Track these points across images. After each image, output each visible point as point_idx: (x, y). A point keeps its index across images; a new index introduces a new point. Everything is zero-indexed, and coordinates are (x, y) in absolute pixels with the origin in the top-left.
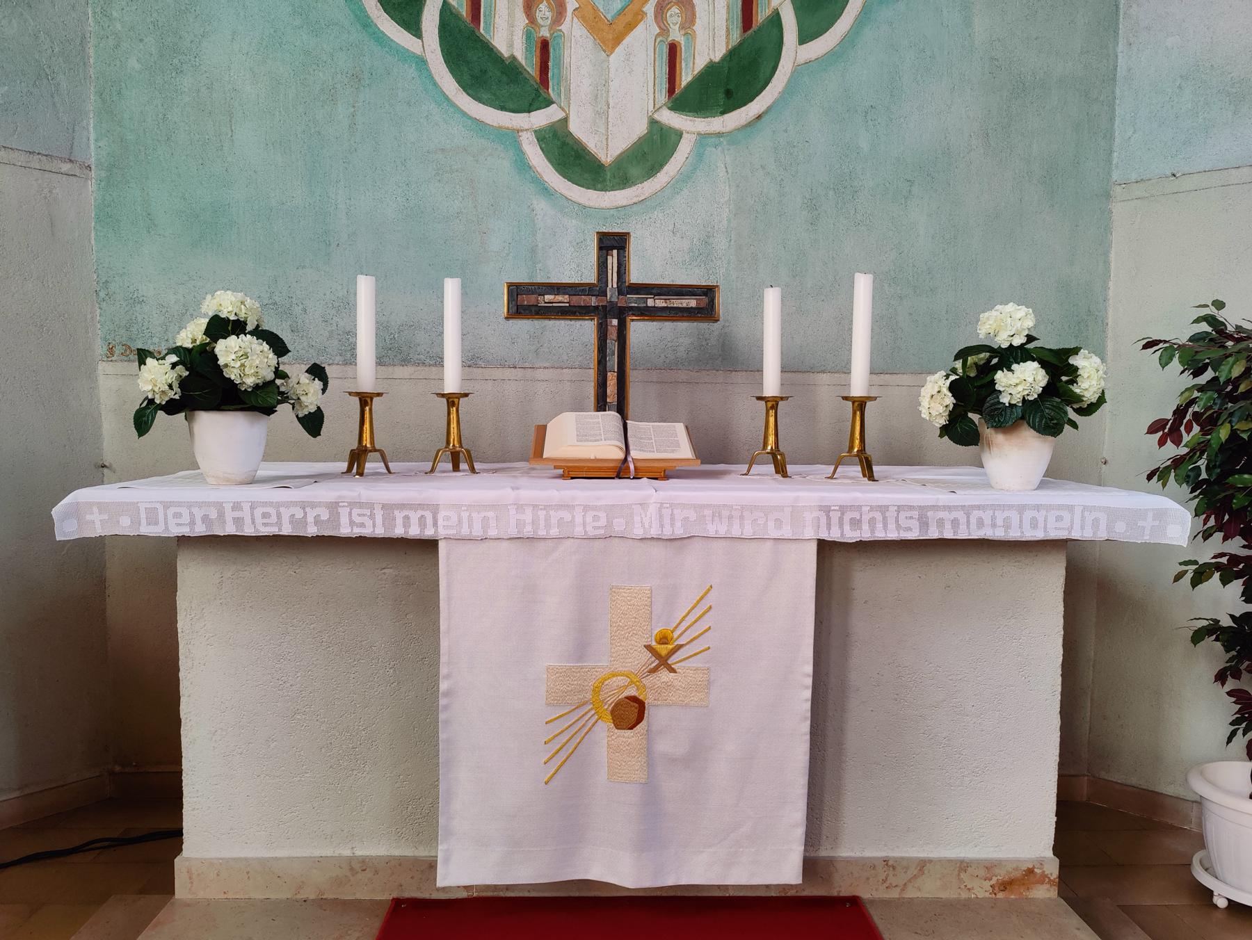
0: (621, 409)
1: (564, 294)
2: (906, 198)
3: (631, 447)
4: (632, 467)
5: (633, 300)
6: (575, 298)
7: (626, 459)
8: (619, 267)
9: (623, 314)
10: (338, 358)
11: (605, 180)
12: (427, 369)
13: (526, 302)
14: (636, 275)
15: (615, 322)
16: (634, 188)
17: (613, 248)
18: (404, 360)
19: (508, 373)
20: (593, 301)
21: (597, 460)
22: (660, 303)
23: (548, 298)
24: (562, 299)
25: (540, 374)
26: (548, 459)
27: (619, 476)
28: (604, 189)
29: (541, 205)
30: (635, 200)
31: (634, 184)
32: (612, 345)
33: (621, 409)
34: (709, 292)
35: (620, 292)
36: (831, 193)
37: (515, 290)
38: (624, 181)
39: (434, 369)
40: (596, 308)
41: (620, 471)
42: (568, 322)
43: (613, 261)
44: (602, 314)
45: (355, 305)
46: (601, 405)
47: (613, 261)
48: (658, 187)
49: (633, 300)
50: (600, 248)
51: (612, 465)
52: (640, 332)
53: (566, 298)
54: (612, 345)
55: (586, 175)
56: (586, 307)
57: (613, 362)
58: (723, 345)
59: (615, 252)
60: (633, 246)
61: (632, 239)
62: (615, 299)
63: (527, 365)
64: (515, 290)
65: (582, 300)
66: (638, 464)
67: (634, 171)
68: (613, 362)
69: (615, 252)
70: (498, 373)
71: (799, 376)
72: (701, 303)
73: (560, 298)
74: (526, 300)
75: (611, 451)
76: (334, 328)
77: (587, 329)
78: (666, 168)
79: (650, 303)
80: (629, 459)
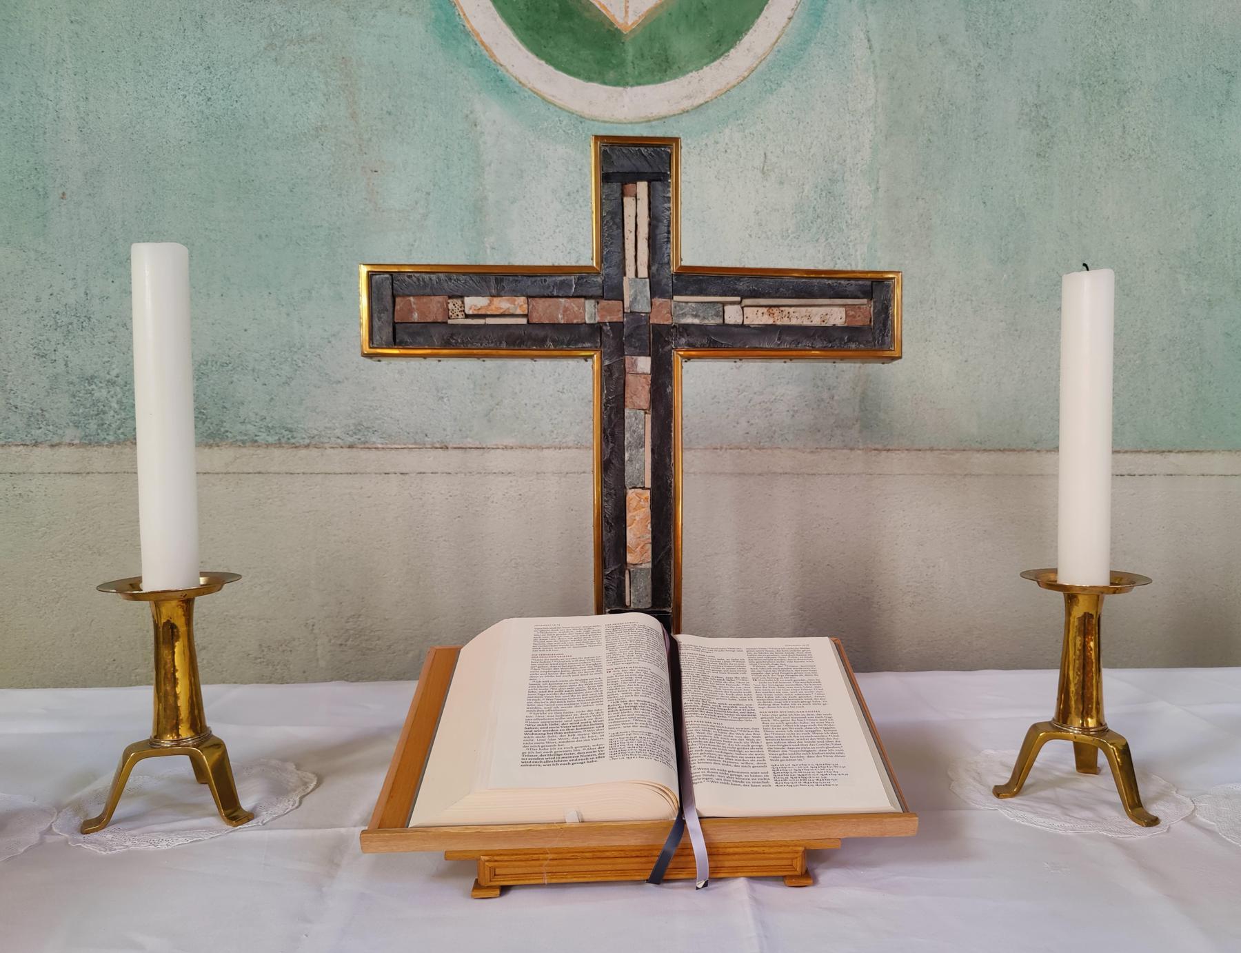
0: (665, 606)
1: (515, 293)
2: (1221, 106)
3: (698, 765)
4: (698, 844)
5: (688, 309)
6: (541, 304)
7: (680, 824)
8: (653, 227)
9: (661, 343)
10: (71, 434)
11: (622, 64)
12: (261, 452)
13: (413, 313)
14: (695, 248)
15: (644, 364)
16: (683, 81)
17: (636, 177)
18: (211, 435)
19: (431, 460)
20: (590, 312)
21: (587, 828)
22: (756, 316)
23: (473, 303)
24: (510, 308)
25: (496, 460)
26: (423, 829)
27: (658, 877)
28: (621, 82)
29: (491, 113)
30: (686, 104)
31: (682, 71)
32: (638, 423)
33: (665, 606)
34: (875, 288)
35: (657, 289)
36: (1077, 93)
37: (389, 287)
38: (662, 66)
39: (277, 452)
40: (597, 329)
41: (662, 860)
42: (528, 363)
43: (636, 208)
44: (613, 341)
45: (127, 325)
46: (610, 599)
47: (636, 208)
48: (732, 78)
49: (688, 309)
50: (606, 178)
51: (634, 841)
52: (701, 381)
53: (518, 304)
54: (638, 423)
55: (584, 53)
56: (569, 327)
57: (639, 463)
58: (863, 400)
59: (642, 187)
60: (691, 172)
61: (684, 151)
62: (643, 307)
63: (469, 442)
64: (389, 287)
65: (560, 310)
66: (724, 837)
67: (682, 45)
68: (639, 463)
69: (642, 187)
70: (410, 460)
71: (1012, 458)
72: (859, 316)
73: (503, 304)
74: (418, 309)
75: (628, 791)
76: (61, 368)
77: (572, 381)
78: (747, 39)
79: (733, 315)
80: (692, 823)
